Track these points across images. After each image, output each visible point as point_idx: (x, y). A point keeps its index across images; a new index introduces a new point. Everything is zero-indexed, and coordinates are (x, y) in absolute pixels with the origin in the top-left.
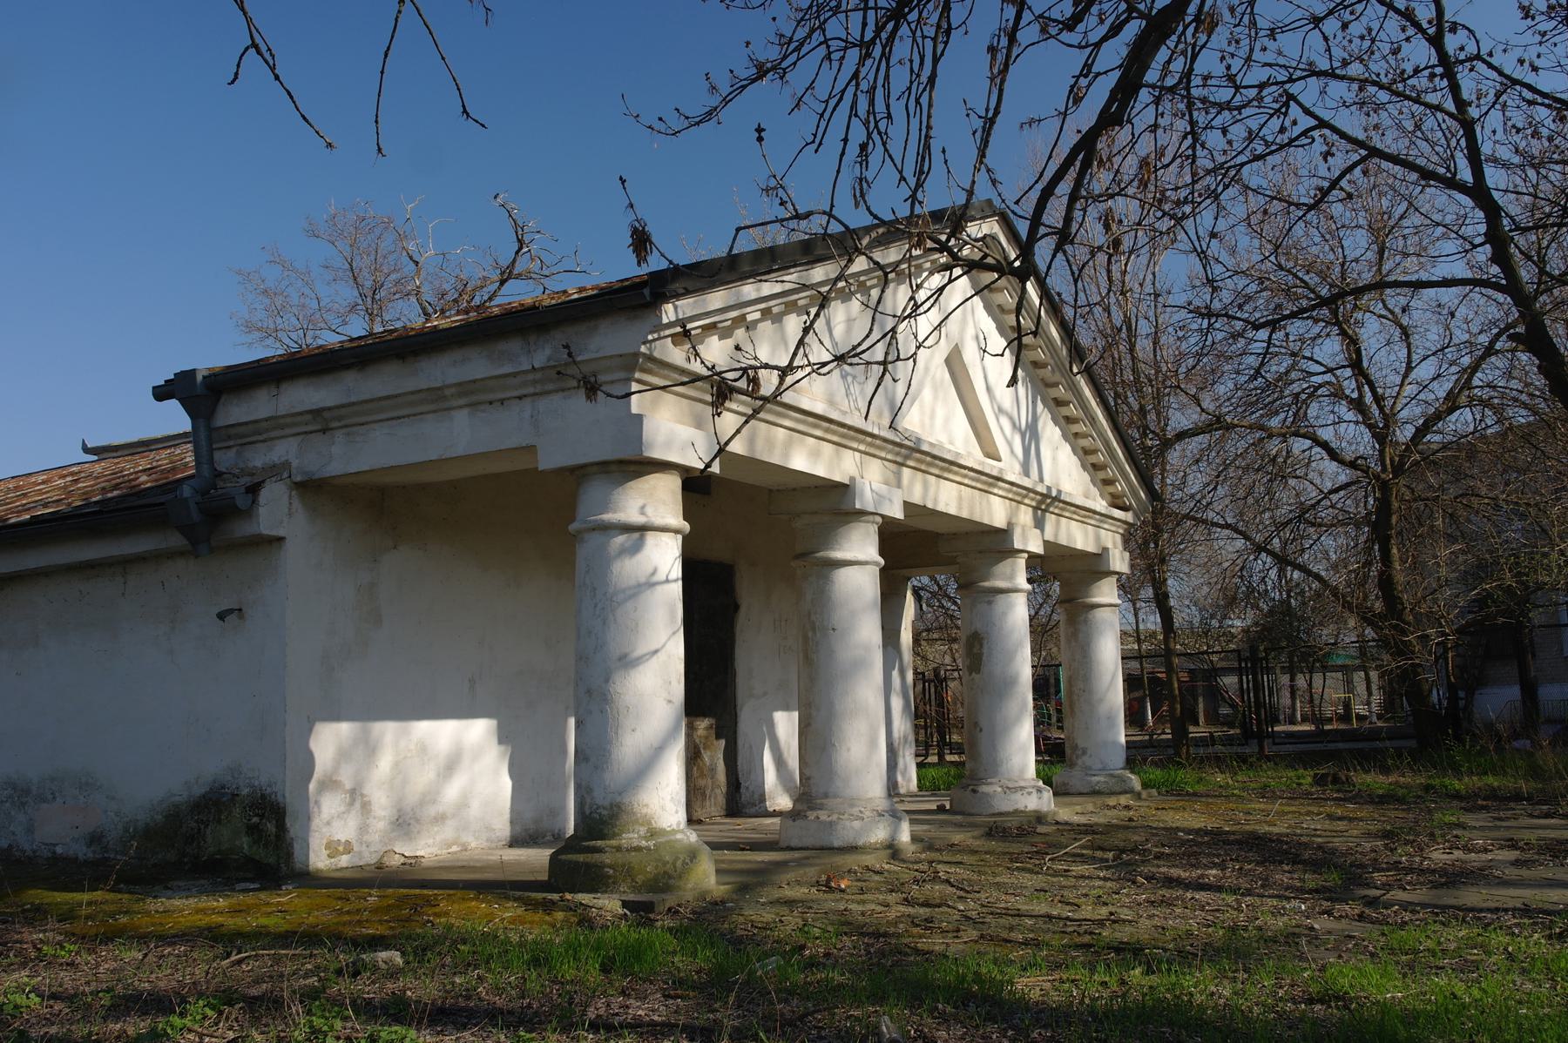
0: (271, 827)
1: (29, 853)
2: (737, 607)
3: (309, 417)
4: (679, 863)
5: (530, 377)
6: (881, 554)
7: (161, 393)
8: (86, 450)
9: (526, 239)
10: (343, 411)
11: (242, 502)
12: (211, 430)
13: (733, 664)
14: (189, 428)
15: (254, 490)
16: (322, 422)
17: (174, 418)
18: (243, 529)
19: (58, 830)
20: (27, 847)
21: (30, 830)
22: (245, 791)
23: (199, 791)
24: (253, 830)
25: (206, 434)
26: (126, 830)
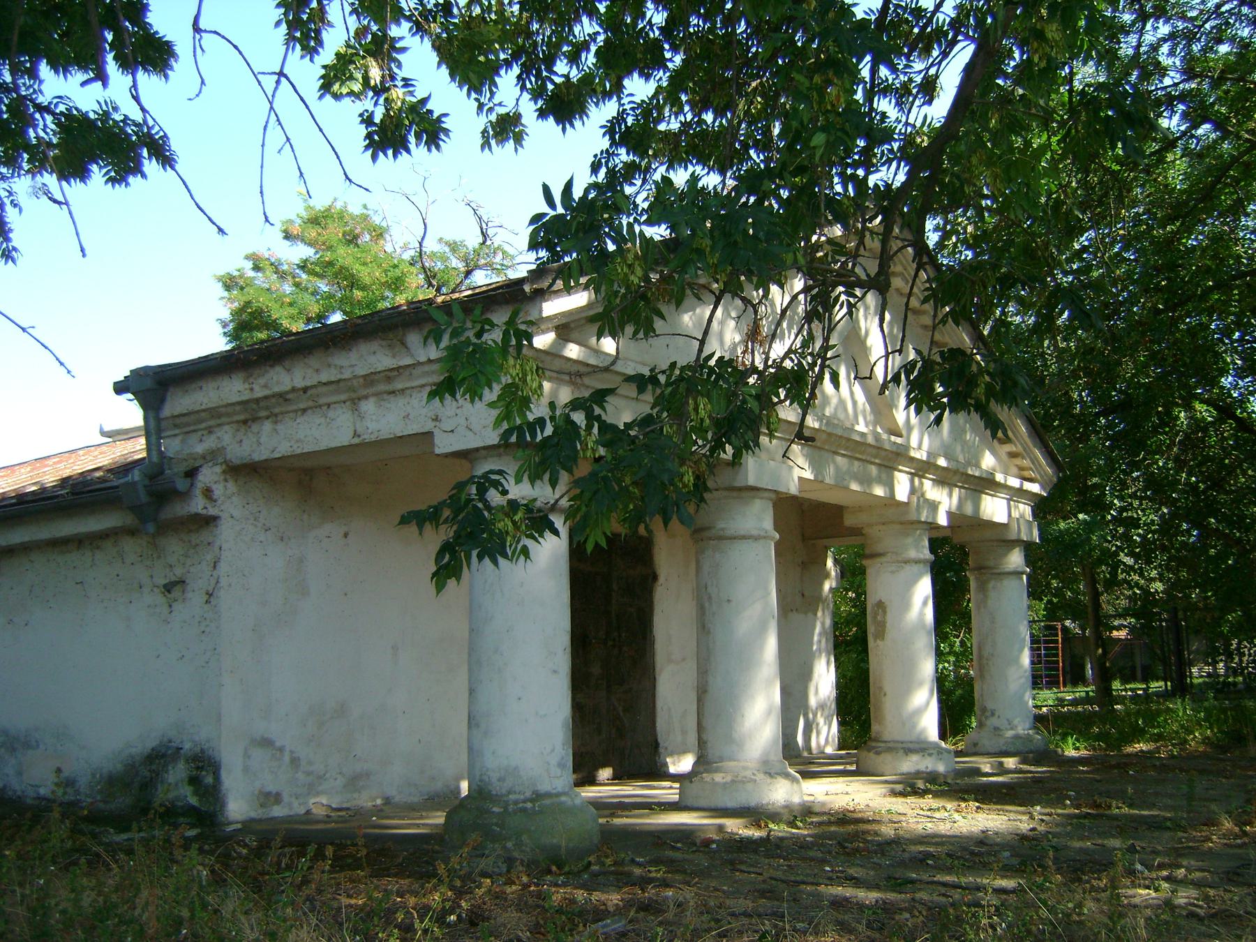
0: (209, 780)
1: (19, 793)
2: (655, 577)
3: (238, 408)
4: (874, 744)
5: (427, 368)
6: (776, 528)
7: (120, 388)
8: (103, 433)
9: (490, 232)
10: (186, 419)
11: (181, 485)
12: (159, 420)
13: (651, 631)
14: (139, 421)
15: (192, 473)
16: (250, 414)
17: (130, 413)
18: (179, 509)
19: (36, 777)
20: (18, 788)
21: (20, 773)
22: (187, 746)
23: (151, 744)
24: (194, 781)
25: (154, 429)
26: (94, 775)
